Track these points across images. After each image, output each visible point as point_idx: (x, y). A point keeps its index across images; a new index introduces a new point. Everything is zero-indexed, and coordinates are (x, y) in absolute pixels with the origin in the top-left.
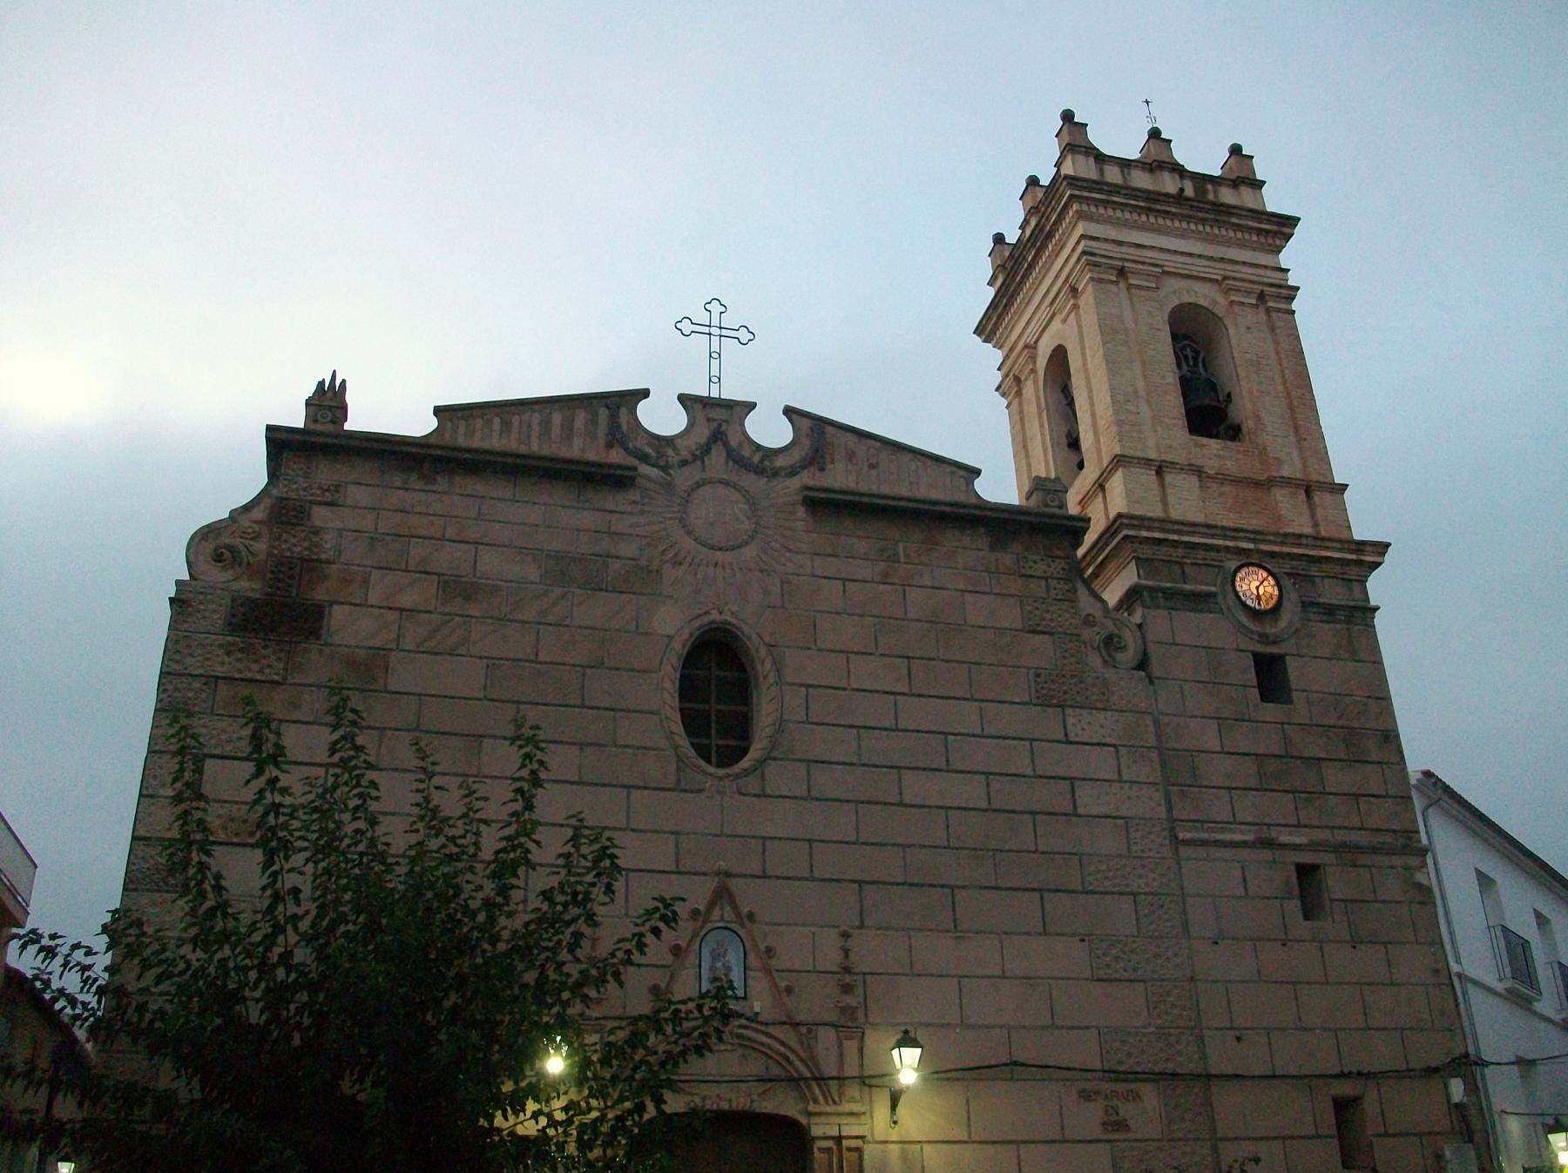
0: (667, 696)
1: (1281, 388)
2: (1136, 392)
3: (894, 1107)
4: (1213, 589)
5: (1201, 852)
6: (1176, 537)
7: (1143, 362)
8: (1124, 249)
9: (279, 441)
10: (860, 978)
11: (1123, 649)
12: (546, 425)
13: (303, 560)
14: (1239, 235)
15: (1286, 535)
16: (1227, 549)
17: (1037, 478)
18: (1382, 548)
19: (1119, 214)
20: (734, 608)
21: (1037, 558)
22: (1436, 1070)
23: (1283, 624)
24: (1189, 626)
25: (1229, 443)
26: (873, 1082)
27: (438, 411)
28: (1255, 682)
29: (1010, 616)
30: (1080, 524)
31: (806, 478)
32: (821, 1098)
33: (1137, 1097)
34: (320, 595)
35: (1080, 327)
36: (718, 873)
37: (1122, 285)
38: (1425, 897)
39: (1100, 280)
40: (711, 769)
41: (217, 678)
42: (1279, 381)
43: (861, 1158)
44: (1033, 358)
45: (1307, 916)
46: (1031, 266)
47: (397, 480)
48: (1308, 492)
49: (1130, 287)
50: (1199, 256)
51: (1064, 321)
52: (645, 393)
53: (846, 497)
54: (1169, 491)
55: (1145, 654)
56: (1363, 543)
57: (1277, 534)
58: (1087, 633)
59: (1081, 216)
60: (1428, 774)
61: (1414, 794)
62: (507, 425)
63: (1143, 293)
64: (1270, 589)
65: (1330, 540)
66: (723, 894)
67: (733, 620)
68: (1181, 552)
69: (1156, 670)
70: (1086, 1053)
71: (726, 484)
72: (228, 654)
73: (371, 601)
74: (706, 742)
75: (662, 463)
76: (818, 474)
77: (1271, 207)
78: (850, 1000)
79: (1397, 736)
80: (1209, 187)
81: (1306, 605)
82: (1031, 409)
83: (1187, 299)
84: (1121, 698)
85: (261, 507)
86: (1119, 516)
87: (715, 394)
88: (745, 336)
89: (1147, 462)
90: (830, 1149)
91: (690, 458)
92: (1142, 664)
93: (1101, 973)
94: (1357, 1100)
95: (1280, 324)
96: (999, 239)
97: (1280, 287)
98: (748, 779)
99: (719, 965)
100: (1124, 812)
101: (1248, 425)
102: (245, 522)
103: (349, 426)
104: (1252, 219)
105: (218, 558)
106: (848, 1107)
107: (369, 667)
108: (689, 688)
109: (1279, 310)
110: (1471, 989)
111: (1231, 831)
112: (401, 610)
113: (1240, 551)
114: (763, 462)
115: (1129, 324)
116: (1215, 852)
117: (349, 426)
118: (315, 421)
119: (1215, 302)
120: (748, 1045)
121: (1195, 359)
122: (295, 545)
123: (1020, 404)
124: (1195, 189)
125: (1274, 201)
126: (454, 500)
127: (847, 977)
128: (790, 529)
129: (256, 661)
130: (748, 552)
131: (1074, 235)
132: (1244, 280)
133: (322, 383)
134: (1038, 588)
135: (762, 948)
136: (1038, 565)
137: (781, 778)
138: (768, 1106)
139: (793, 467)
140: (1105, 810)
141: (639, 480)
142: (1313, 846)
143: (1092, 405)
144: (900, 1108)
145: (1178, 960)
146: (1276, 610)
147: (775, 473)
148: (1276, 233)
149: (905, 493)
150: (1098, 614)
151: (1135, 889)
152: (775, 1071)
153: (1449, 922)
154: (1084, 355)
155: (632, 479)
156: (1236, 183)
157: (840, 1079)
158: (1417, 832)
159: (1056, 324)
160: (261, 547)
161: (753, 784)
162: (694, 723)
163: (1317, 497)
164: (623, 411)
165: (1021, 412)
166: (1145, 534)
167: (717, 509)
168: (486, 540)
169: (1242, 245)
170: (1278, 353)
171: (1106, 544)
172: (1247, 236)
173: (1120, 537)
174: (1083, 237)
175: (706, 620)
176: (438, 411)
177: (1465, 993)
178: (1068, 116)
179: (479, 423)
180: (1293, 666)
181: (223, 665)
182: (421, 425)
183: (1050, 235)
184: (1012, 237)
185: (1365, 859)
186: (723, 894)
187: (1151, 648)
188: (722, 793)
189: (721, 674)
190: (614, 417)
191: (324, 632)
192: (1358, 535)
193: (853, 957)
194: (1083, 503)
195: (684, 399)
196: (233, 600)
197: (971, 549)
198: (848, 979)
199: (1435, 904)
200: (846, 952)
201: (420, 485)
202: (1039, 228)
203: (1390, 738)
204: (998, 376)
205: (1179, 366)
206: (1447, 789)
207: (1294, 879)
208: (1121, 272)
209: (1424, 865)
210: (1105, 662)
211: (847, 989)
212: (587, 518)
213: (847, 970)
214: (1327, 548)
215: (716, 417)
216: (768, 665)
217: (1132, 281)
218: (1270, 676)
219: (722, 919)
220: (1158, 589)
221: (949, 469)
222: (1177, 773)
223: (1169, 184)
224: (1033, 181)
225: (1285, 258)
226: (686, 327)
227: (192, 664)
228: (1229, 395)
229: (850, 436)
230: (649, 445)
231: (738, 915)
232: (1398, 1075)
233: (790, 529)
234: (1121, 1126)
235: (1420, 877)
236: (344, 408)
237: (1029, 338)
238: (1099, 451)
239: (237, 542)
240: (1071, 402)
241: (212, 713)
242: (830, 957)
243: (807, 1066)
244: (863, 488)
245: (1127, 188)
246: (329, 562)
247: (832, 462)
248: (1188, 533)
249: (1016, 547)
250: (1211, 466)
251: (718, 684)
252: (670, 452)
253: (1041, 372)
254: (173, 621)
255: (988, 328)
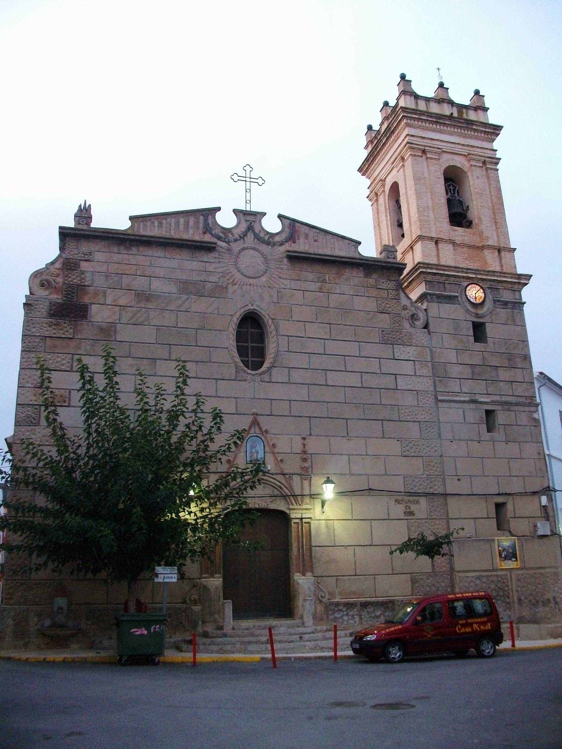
0: (231, 342)
1: (490, 205)
2: (428, 207)
3: (323, 507)
4: (457, 294)
5: (447, 405)
6: (442, 272)
7: (432, 194)
8: (425, 141)
9: (65, 235)
10: (309, 455)
11: (418, 320)
12: (177, 224)
13: (78, 285)
14: (476, 134)
15: (489, 271)
16: (464, 277)
17: (385, 245)
18: (529, 277)
19: (424, 124)
20: (258, 304)
21: (384, 281)
22: (536, 492)
23: (485, 309)
24: (446, 310)
25: (467, 230)
26: (315, 496)
27: (131, 218)
28: (472, 334)
29: (372, 305)
30: (403, 266)
31: (287, 247)
32: (294, 503)
33: (417, 502)
34: (86, 300)
35: (405, 175)
36: (253, 414)
37: (424, 157)
38: (536, 423)
39: (415, 155)
40: (249, 371)
41: (46, 337)
42: (490, 201)
43: (310, 526)
44: (384, 186)
45: (489, 431)
46: (384, 144)
47: (115, 250)
48: (499, 251)
49: (427, 158)
50: (458, 144)
51: (398, 171)
52: (219, 209)
53: (304, 255)
54: (440, 251)
55: (427, 322)
56: (521, 275)
57: (485, 271)
58: (404, 313)
59: (408, 125)
60: (541, 373)
61: (535, 381)
62: (160, 224)
63: (433, 161)
64: (481, 294)
65: (508, 274)
66: (255, 423)
67: (258, 309)
68: (444, 278)
69: (431, 327)
70: (398, 485)
71: (254, 249)
72: (50, 326)
73: (108, 302)
74: (247, 359)
75: (227, 240)
76: (292, 244)
77: (491, 122)
78: (306, 465)
79: (530, 357)
80: (464, 110)
81: (495, 301)
82: (382, 208)
83: (452, 164)
84: (417, 340)
85: (59, 262)
86: (419, 263)
87: (248, 209)
88: (261, 181)
89: (431, 238)
90: (298, 523)
91: (239, 238)
92: (426, 327)
93: (405, 454)
94: (504, 504)
95: (491, 175)
96: (370, 128)
97: (493, 158)
98: (265, 375)
99: (254, 451)
100: (417, 388)
101: (475, 221)
102: (52, 269)
103: (93, 225)
104: (483, 127)
105: (42, 285)
106: (304, 506)
107: (108, 331)
108: (240, 337)
109: (491, 169)
110: (553, 461)
111: (459, 396)
112: (121, 306)
113: (469, 278)
114: (269, 239)
115: (426, 175)
116: (452, 405)
117: (93, 225)
118: (79, 224)
119: (464, 165)
120: (267, 483)
121: (454, 190)
122: (74, 279)
123: (377, 205)
124: (458, 112)
125: (493, 118)
126: (139, 257)
127: (305, 455)
128: (281, 269)
129: (61, 330)
130: (264, 279)
131: (404, 133)
132: (477, 155)
133: (80, 206)
134: (384, 294)
135: (271, 444)
136: (385, 284)
137: (278, 375)
138: (273, 506)
139: (282, 241)
140: (409, 387)
141: (218, 248)
142: (493, 403)
143: (409, 211)
144: (326, 507)
145: (436, 448)
146: (483, 303)
147: (274, 244)
148: (492, 133)
149: (329, 253)
150: (409, 305)
151: (420, 420)
152: (276, 492)
153: (546, 437)
154: (406, 188)
155: (215, 248)
156: (476, 109)
157: (302, 495)
158: (535, 397)
159: (395, 171)
160: (60, 280)
161: (266, 377)
162: (242, 352)
163: (503, 254)
164: (210, 217)
165: (378, 209)
166: (429, 271)
167: (250, 260)
168: (153, 275)
169: (477, 138)
170: (490, 188)
171: (413, 274)
172: (479, 134)
173: (419, 271)
174: (408, 135)
175: (247, 308)
176: (131, 218)
177: (550, 462)
178: (403, 77)
179: (149, 223)
180: (489, 328)
181: (48, 331)
182: (124, 225)
183: (393, 132)
184: (376, 127)
185: (513, 408)
186: (255, 423)
187: (430, 320)
188: (254, 381)
189: (252, 330)
190: (206, 220)
191: (89, 316)
192: (519, 271)
193: (307, 448)
194: (404, 253)
195: (235, 211)
196: (50, 303)
197: (355, 277)
198: (305, 456)
199: (540, 426)
200: (304, 445)
201: (125, 252)
202: (388, 128)
203: (527, 358)
204: (368, 192)
205: (447, 193)
206: (549, 379)
207: (484, 416)
208: (424, 152)
209: (537, 411)
210: (411, 325)
211: (305, 460)
212: (195, 265)
213: (305, 452)
214: (505, 277)
215: (249, 218)
216: (272, 327)
217: (428, 156)
218: (479, 331)
219: (255, 433)
220: (434, 294)
221: (347, 241)
222: (439, 372)
223: (446, 110)
224: (386, 104)
225: (496, 145)
226: (236, 178)
227: (35, 331)
228: (468, 206)
229: (307, 227)
230: (222, 232)
231: (261, 430)
232: (520, 494)
233: (281, 269)
234: (412, 513)
235: (535, 416)
236: (91, 218)
237: (382, 176)
238: (411, 232)
239: (49, 278)
240: (400, 208)
241: (45, 352)
242: (298, 448)
243: (289, 491)
244: (311, 251)
245: (428, 113)
246: (88, 286)
247: (299, 239)
248: (448, 270)
249: (375, 276)
250: (458, 240)
251: (252, 332)
252: (230, 236)
253: (387, 193)
254: (26, 313)
255: (364, 169)
